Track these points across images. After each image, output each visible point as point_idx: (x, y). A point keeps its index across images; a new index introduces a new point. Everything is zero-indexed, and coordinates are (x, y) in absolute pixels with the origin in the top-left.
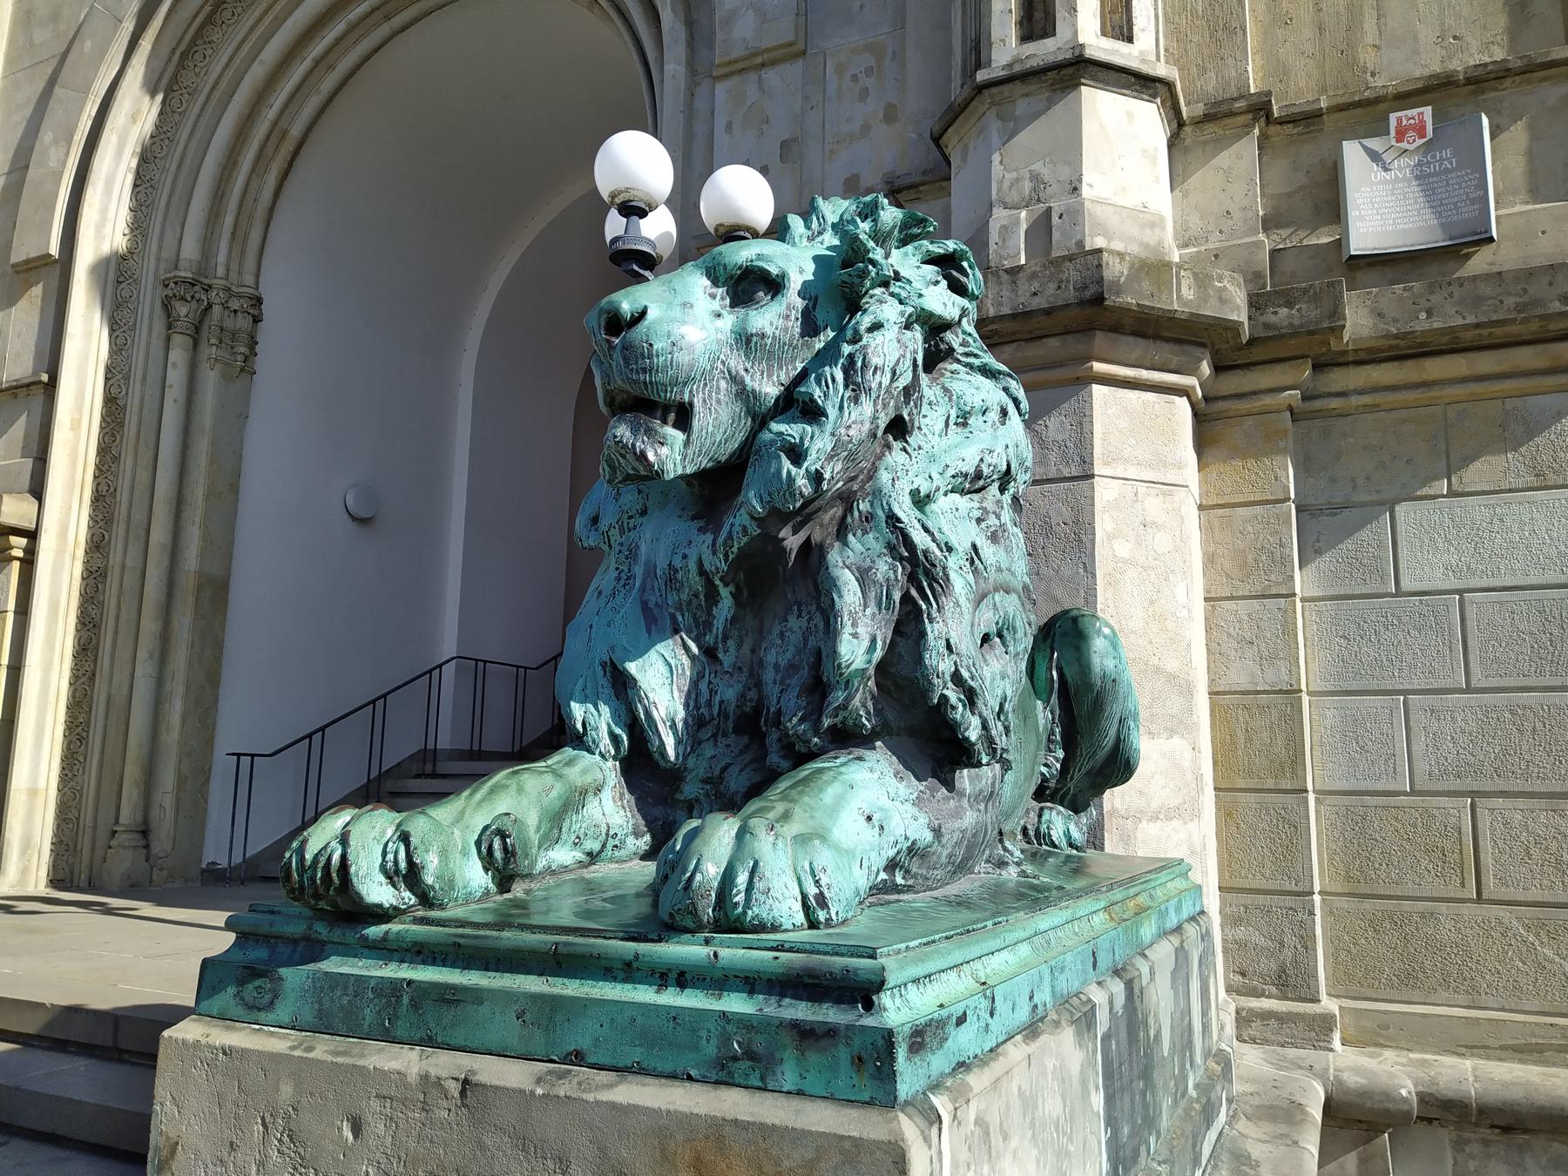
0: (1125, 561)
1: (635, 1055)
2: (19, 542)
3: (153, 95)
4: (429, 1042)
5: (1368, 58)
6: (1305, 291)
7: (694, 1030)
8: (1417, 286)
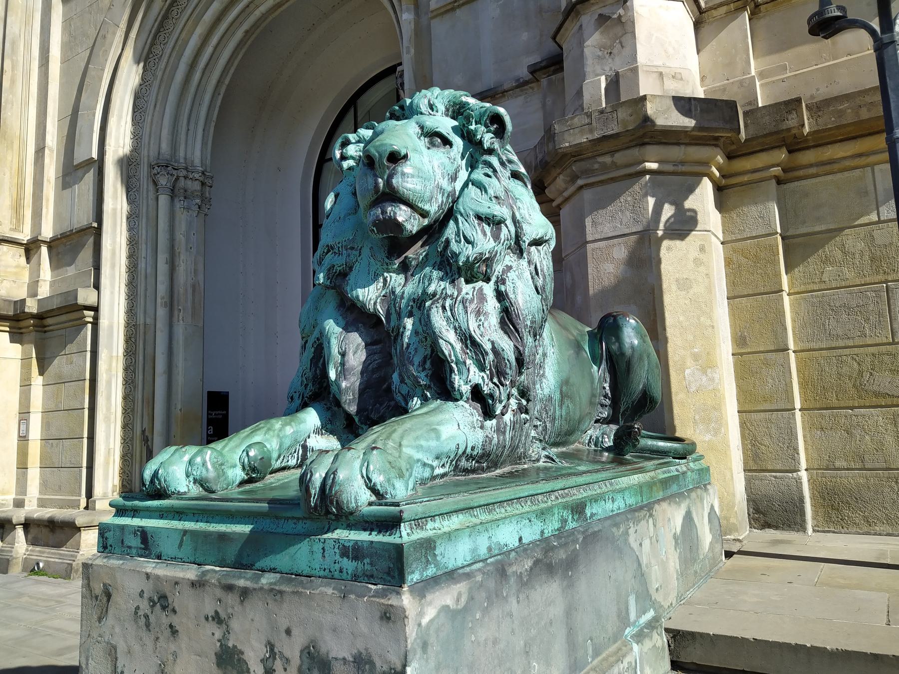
2: (89, 314)
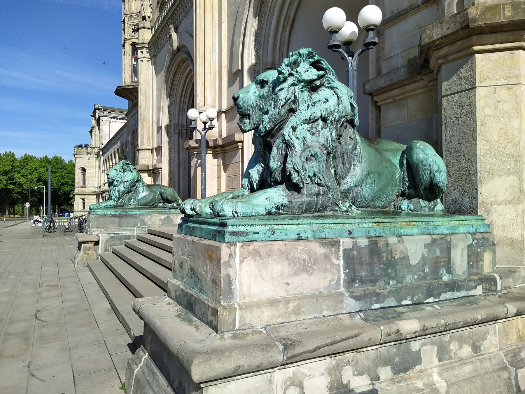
0: (489, 116)
2: (240, 144)
3: (256, 18)
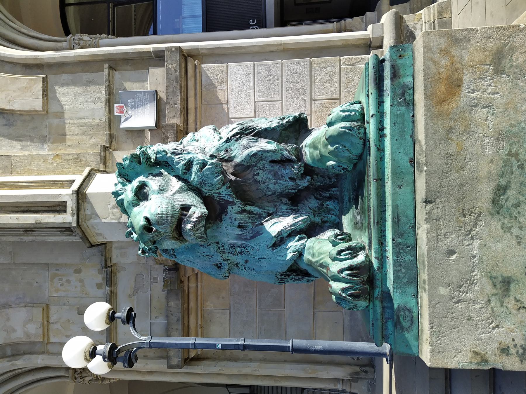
1: (408, 137)
4: (414, 227)
5: (96, 121)
6: (164, 134)
7: (397, 116)
8: (167, 107)
